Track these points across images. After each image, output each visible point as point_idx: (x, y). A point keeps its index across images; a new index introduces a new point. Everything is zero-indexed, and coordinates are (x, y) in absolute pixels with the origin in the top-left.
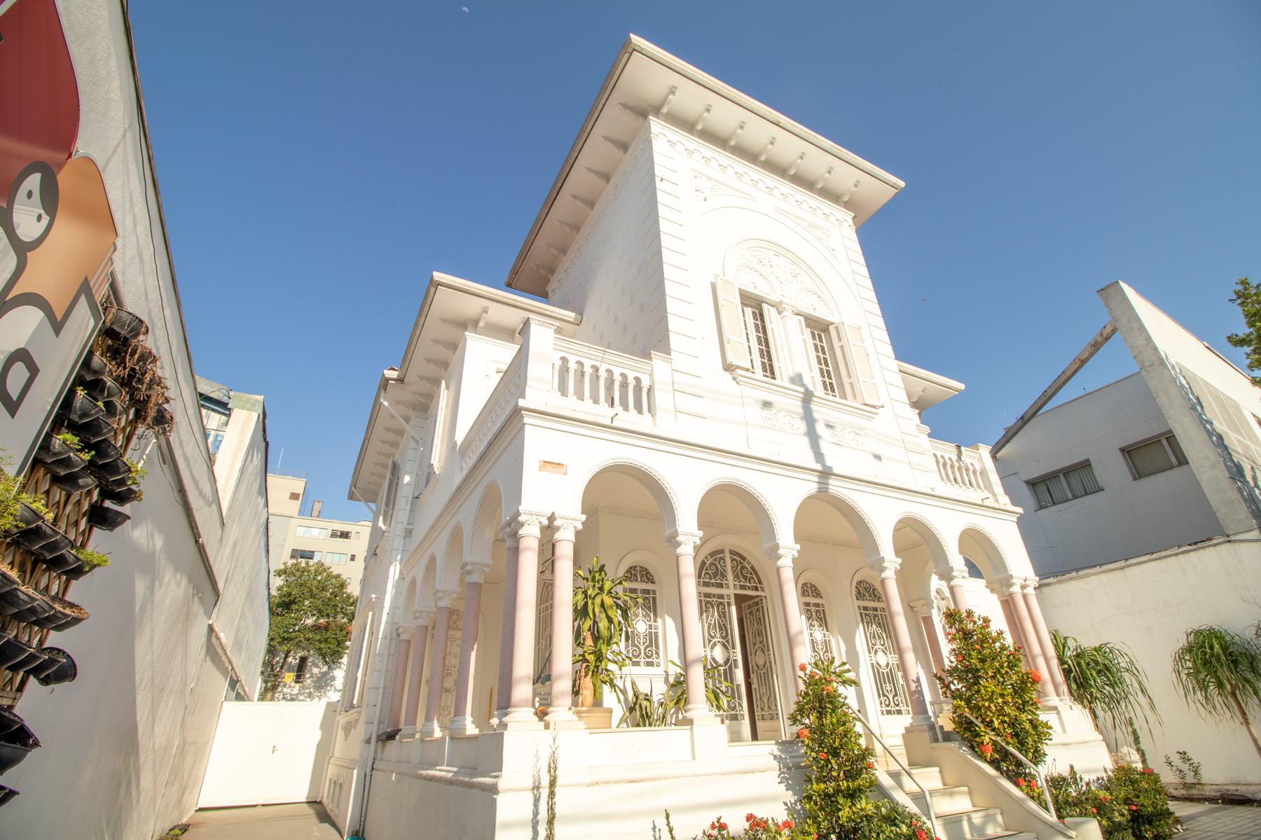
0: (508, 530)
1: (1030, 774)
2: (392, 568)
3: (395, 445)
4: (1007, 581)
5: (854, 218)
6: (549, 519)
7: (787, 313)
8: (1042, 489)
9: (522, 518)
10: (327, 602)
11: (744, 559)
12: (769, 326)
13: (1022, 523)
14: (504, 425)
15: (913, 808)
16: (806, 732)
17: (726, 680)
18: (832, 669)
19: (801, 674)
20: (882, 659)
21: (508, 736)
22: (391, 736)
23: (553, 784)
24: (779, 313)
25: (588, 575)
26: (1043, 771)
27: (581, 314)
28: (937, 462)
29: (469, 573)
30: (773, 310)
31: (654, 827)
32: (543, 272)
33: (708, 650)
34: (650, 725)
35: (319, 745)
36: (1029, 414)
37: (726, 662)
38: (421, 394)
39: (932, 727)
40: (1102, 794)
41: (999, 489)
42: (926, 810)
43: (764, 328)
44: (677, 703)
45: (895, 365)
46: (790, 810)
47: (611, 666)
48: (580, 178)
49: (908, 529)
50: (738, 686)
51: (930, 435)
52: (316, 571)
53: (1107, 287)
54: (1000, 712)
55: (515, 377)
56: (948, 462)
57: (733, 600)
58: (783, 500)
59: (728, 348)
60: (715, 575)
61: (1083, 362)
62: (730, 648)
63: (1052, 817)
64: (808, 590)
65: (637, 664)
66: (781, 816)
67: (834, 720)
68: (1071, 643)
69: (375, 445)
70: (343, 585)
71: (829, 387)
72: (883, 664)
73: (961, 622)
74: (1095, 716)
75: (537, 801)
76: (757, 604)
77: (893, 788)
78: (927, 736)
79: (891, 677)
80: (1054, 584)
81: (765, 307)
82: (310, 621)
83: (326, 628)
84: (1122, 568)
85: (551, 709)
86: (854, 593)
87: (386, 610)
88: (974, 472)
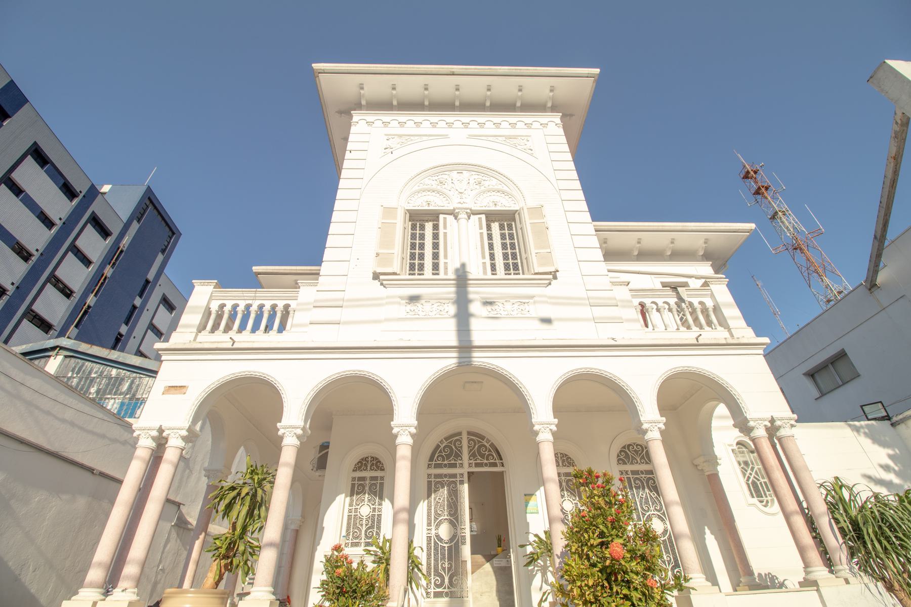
11: (483, 438)
33: (433, 527)
37: (451, 540)
53: (875, 72)
60: (448, 457)
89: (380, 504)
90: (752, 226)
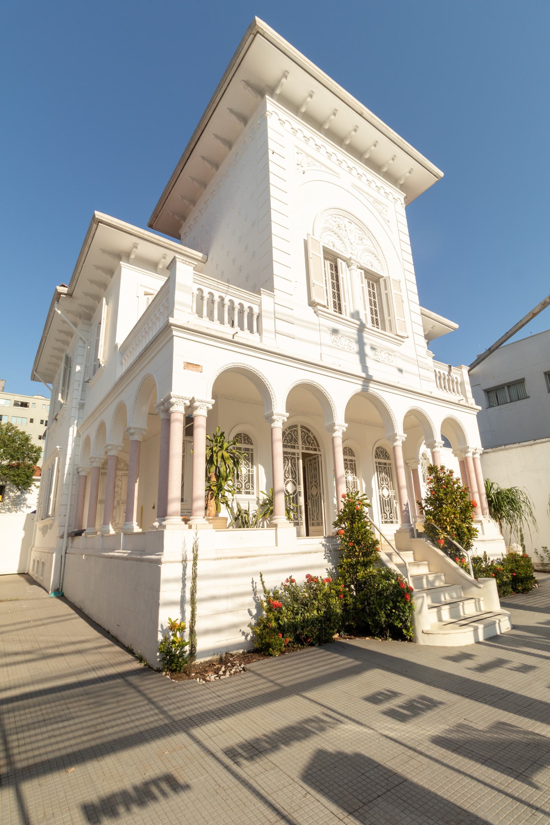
0: (162, 407)
1: (463, 555)
2: (71, 429)
3: (67, 343)
4: (465, 450)
5: (405, 198)
6: (190, 401)
7: (354, 267)
8: (493, 395)
9: (173, 400)
10: (16, 450)
11: (309, 431)
12: (340, 276)
13: (480, 416)
14: (156, 335)
15: (398, 571)
16: (343, 531)
17: (293, 502)
18: (357, 498)
19: (343, 500)
20: (386, 492)
21: (167, 533)
22: (79, 533)
23: (195, 558)
24: (348, 267)
25: (213, 438)
26: (469, 555)
27: (207, 255)
28: (436, 375)
29: (132, 434)
30: (344, 264)
31: (253, 582)
32: (177, 218)
33: (381, 490)
34: (248, 527)
35: (23, 540)
36: (495, 347)
37: (294, 493)
38: (86, 307)
39: (412, 530)
40: (499, 567)
41: (469, 394)
42: (406, 572)
43: (337, 277)
44: (264, 515)
45: (417, 308)
46: (330, 573)
47: (227, 494)
48: (208, 143)
49: (412, 417)
50: (300, 506)
51: (434, 358)
52: (7, 429)
54: (452, 522)
55: (164, 300)
56: (442, 376)
57: (301, 456)
58: (341, 395)
59: (313, 289)
60: (291, 441)
61: (534, 315)
62: (297, 484)
63: (471, 577)
64: (348, 451)
65: (240, 492)
66: (325, 576)
67: (360, 525)
68: (495, 486)
69: (50, 343)
70: (27, 439)
71: (375, 322)
72: (386, 495)
73: (436, 472)
74: (501, 525)
75: (185, 568)
76: (315, 459)
77: (388, 561)
78: (408, 535)
79: (390, 503)
80: (490, 452)
81: (339, 261)
82: (5, 463)
83: (18, 466)
84: (531, 445)
85: (192, 517)
86: (374, 454)
87: (69, 456)
88: (457, 383)
89: (252, 468)
90: (456, 326)
